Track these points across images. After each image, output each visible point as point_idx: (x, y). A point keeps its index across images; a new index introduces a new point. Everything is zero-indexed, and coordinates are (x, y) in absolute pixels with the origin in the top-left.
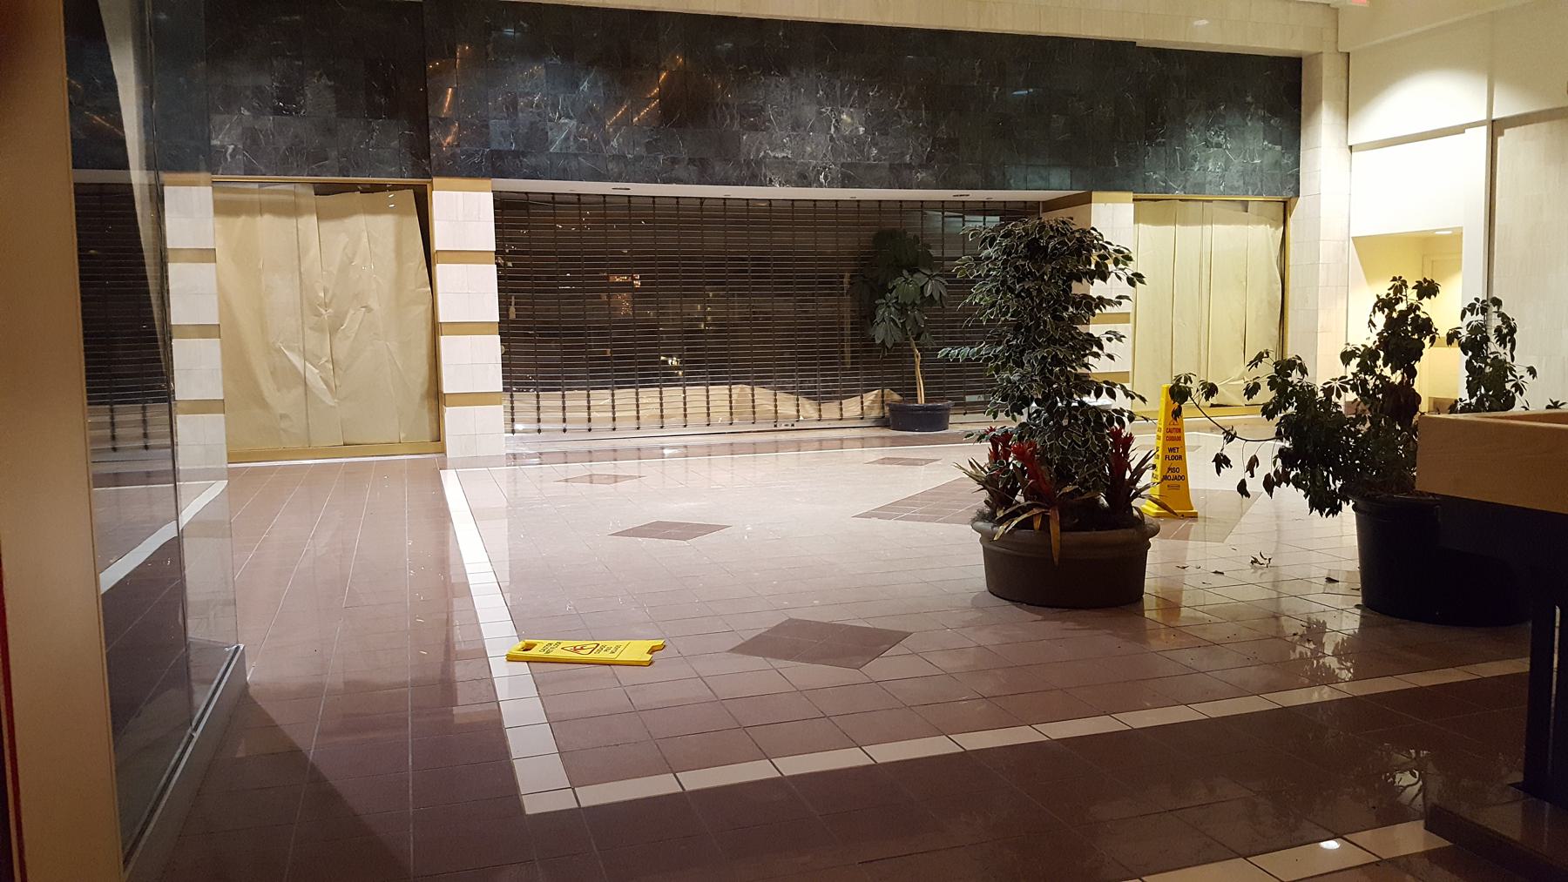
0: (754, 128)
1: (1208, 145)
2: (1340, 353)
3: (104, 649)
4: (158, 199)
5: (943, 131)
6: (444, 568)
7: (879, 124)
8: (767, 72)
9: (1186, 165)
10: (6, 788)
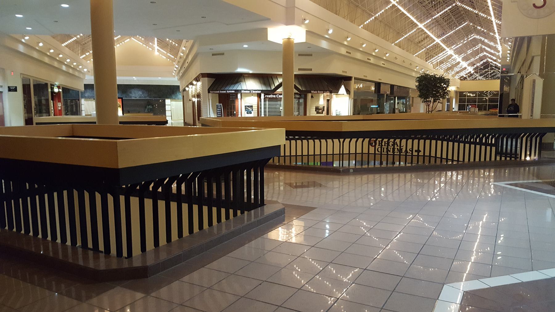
0: (131, 93)
1: (179, 94)
2: (533, 7)
3: (435, 57)
4: (81, 99)
5: (149, 93)
6: (422, 41)
7: (143, 93)
8: (132, 89)
9: (177, 96)
10: (41, 221)
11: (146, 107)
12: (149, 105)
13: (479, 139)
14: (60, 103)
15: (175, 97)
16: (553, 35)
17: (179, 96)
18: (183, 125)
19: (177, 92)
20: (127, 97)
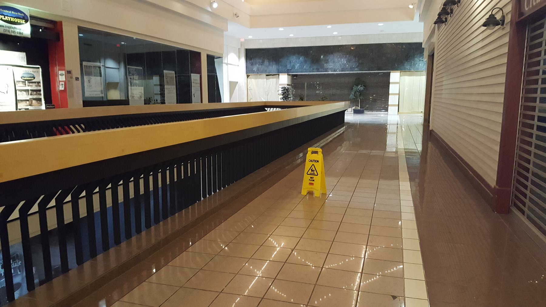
0: (327, 63)
1: (420, 61)
7: (349, 61)
8: (329, 54)
9: (414, 65)
11: (352, 89)
12: (357, 85)
13: (61, 192)
14: (63, 72)
15: (411, 66)
16: (545, 117)
17: (419, 65)
18: (280, 74)
19: (415, 56)
20: (320, 70)
